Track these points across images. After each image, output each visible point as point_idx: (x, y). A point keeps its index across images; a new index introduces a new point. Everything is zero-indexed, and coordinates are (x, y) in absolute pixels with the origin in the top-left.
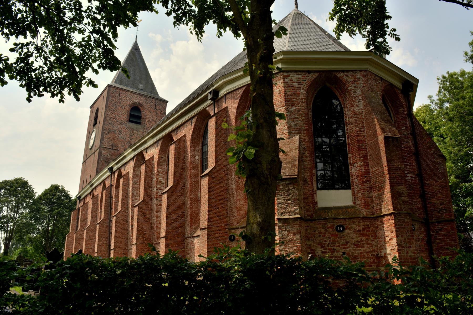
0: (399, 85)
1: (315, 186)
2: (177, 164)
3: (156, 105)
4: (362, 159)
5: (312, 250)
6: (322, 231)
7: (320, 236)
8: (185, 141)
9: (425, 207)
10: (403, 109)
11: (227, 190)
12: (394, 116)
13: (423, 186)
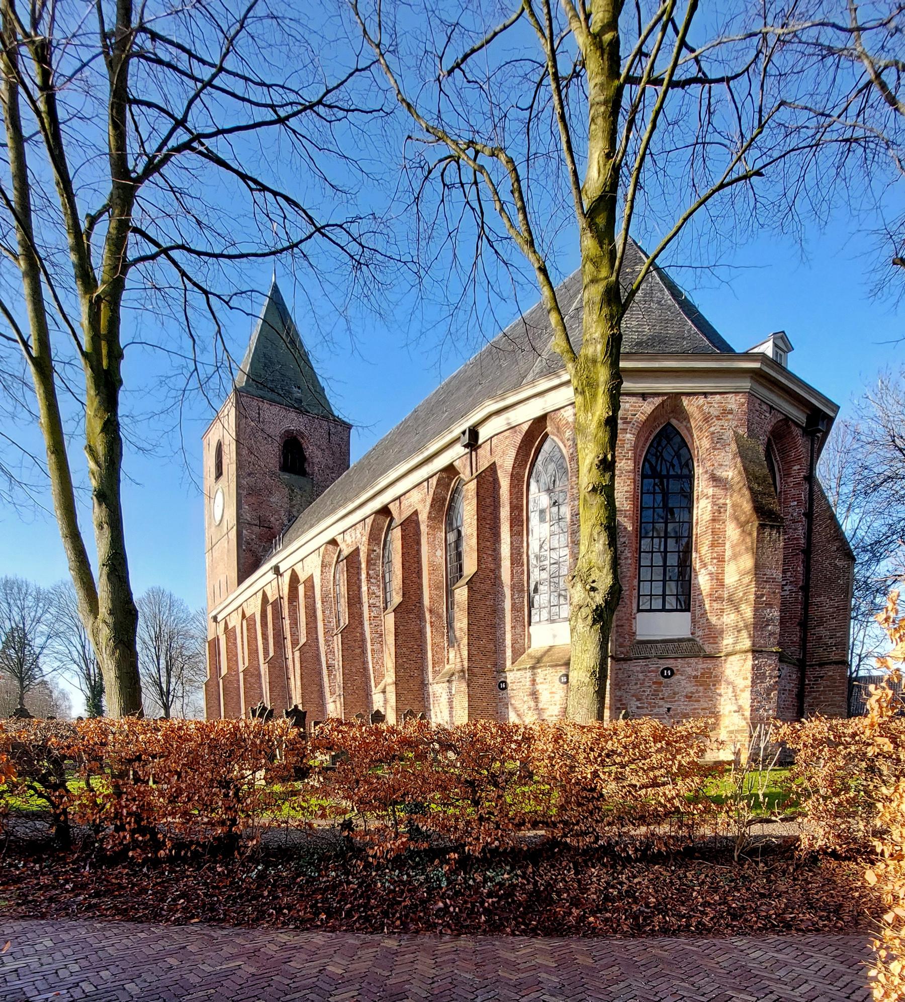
0: (799, 416)
1: (635, 606)
2: (407, 564)
3: (329, 434)
4: (715, 561)
5: (624, 704)
6: (641, 676)
7: (636, 684)
8: (417, 523)
9: (804, 640)
10: (799, 467)
11: (495, 611)
12: (781, 478)
13: (806, 605)
